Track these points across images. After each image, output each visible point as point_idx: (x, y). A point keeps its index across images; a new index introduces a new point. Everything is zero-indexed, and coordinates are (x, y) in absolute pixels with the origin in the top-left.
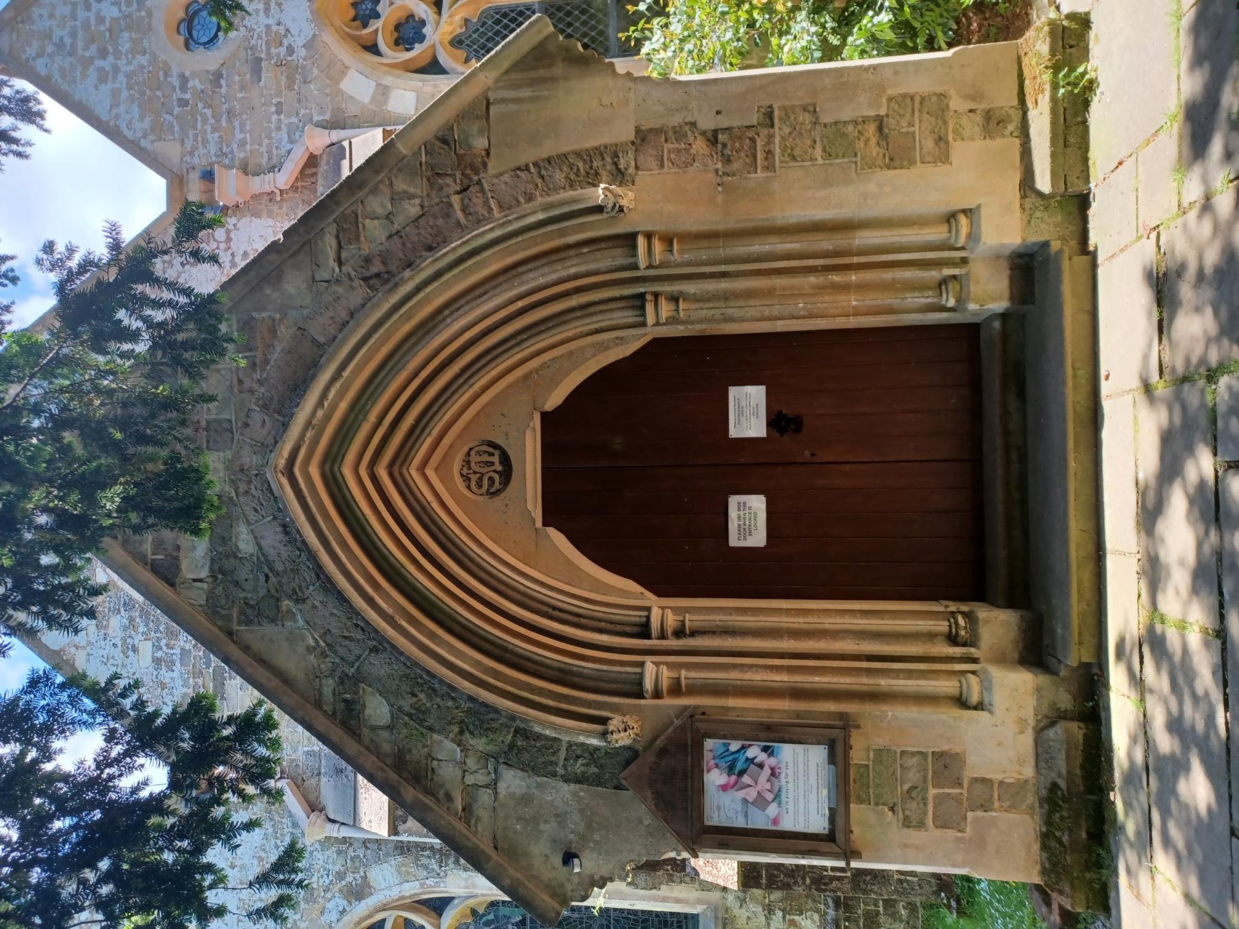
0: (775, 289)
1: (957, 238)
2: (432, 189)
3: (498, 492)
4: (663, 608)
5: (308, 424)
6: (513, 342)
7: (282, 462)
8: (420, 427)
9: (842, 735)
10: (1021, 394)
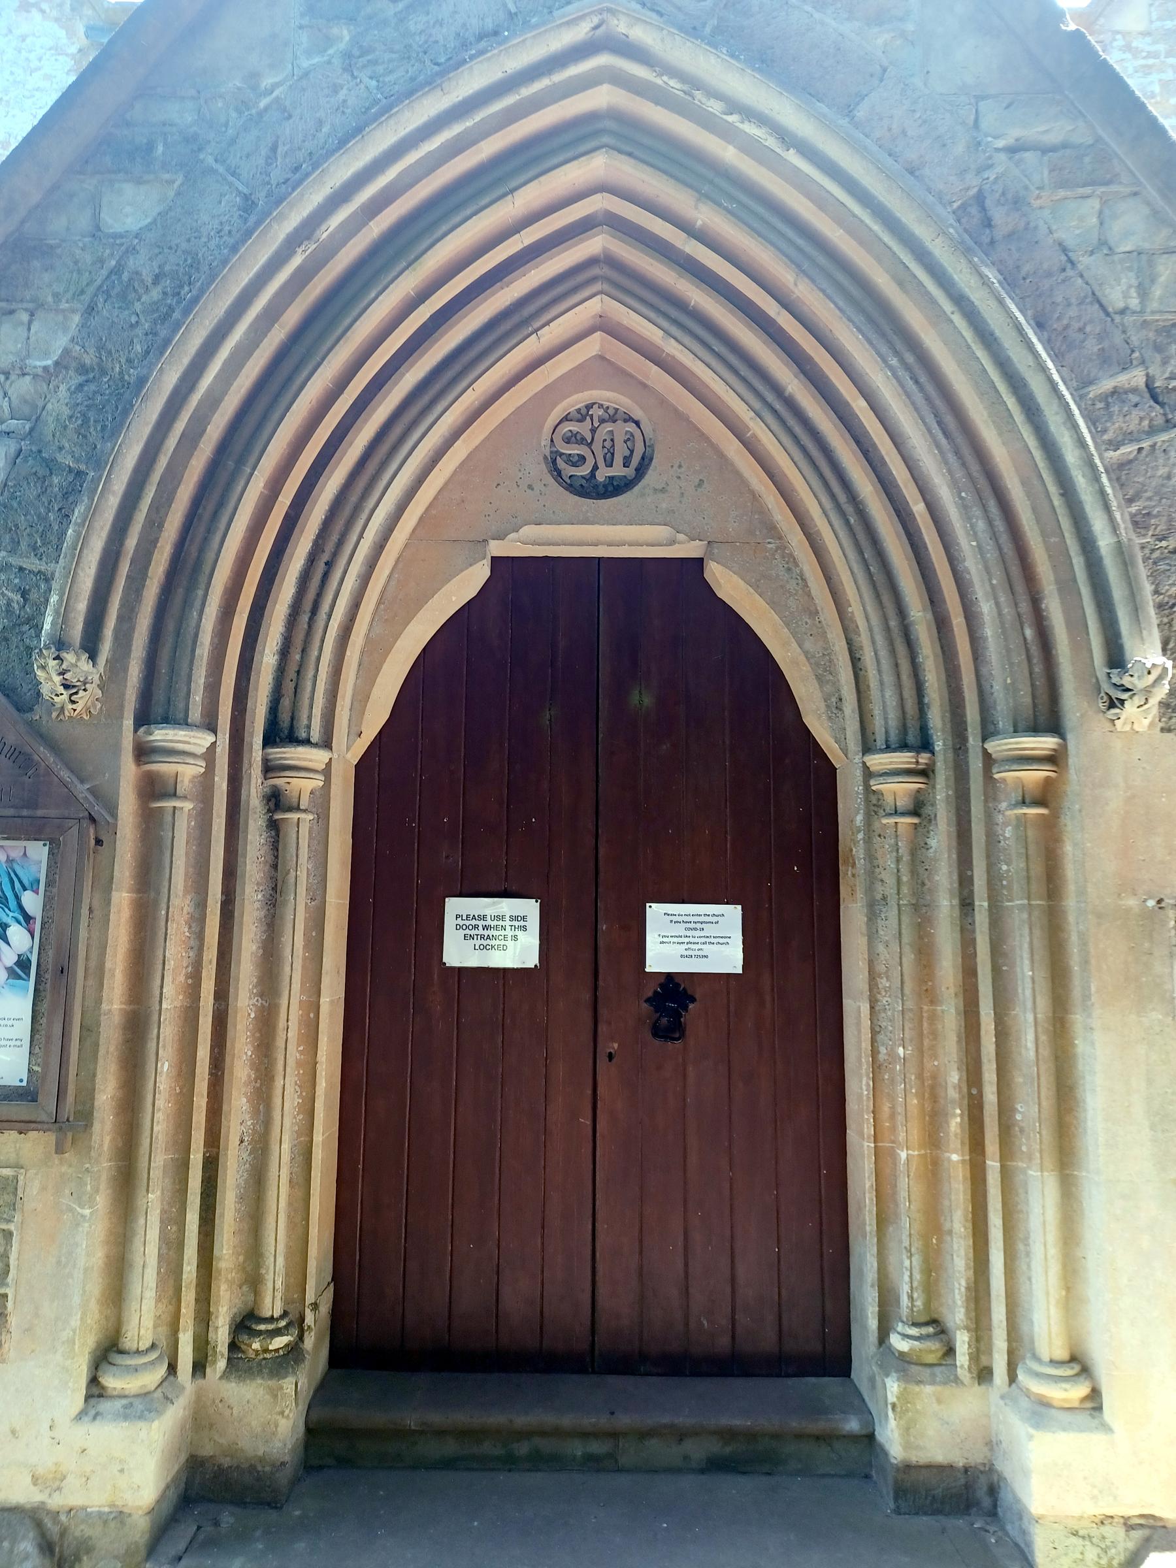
0: (933, 1002)
1: (1038, 1375)
2: (1158, 332)
3: (557, 473)
4: (327, 771)
5: (693, 83)
6: (842, 497)
7: (621, 26)
8: (683, 318)
9: (44, 1117)
10: (717, 1465)
